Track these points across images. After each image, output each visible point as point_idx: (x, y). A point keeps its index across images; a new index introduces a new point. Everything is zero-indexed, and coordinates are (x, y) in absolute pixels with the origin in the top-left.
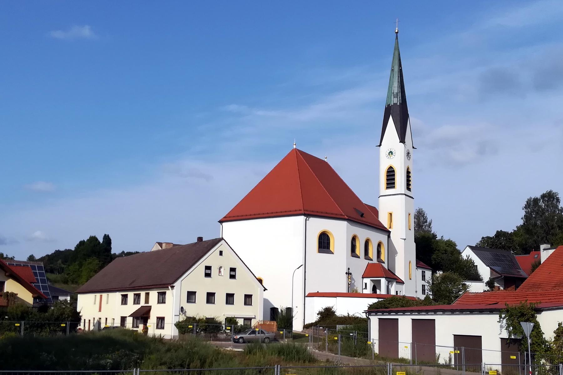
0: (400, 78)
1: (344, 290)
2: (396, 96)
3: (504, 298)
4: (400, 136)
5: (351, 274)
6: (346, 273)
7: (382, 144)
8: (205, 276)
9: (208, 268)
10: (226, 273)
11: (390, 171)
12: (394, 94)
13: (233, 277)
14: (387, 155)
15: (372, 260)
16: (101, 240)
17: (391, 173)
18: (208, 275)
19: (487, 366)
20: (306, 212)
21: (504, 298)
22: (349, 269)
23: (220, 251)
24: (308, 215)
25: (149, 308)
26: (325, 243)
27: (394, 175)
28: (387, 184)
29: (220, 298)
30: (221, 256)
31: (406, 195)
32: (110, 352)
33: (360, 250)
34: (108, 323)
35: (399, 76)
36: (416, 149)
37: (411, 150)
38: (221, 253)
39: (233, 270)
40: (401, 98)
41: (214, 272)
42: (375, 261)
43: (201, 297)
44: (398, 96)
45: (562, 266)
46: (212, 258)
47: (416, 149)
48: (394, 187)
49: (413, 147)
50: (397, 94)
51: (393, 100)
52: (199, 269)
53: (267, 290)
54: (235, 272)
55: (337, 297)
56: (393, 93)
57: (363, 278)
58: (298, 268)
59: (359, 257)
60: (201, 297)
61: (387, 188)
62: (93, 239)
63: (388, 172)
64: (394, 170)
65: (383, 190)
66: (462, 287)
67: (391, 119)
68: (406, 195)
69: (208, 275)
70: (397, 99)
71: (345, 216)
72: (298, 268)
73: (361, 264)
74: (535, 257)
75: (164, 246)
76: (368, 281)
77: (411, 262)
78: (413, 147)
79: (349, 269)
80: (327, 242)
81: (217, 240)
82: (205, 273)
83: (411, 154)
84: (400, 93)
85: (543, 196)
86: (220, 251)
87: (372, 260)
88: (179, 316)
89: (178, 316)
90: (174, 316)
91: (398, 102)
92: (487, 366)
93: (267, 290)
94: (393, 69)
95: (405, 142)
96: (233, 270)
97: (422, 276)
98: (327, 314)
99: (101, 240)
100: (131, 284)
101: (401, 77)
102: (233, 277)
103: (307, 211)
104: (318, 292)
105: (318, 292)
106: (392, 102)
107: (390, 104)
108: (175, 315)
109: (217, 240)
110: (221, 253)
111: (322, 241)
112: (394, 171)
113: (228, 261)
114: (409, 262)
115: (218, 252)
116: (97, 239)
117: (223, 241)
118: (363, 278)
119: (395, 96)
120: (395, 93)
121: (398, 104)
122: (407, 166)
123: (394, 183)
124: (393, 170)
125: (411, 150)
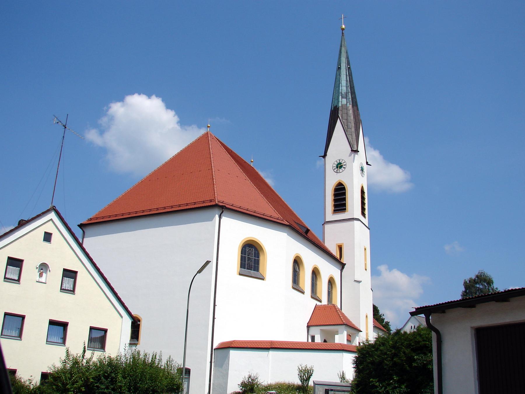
0: (349, 77)
11: (341, 209)
12: (342, 94)
14: (334, 168)
15: (320, 301)
19: (54, 341)
26: (251, 261)
28: (335, 206)
34: (16, 335)
35: (348, 74)
36: (371, 165)
37: (365, 166)
38: (48, 237)
42: (325, 302)
47: (371, 165)
49: (367, 163)
50: (347, 93)
58: (200, 271)
59: (303, 293)
61: (334, 211)
63: (336, 190)
64: (345, 187)
65: (330, 216)
66: (393, 379)
72: (200, 271)
77: (368, 316)
78: (367, 163)
83: (365, 170)
84: (350, 94)
87: (320, 301)
92: (54, 341)
94: (339, 66)
95: (359, 152)
101: (351, 83)
107: (337, 106)
110: (48, 237)
112: (344, 189)
114: (364, 249)
120: (343, 93)
125: (365, 166)
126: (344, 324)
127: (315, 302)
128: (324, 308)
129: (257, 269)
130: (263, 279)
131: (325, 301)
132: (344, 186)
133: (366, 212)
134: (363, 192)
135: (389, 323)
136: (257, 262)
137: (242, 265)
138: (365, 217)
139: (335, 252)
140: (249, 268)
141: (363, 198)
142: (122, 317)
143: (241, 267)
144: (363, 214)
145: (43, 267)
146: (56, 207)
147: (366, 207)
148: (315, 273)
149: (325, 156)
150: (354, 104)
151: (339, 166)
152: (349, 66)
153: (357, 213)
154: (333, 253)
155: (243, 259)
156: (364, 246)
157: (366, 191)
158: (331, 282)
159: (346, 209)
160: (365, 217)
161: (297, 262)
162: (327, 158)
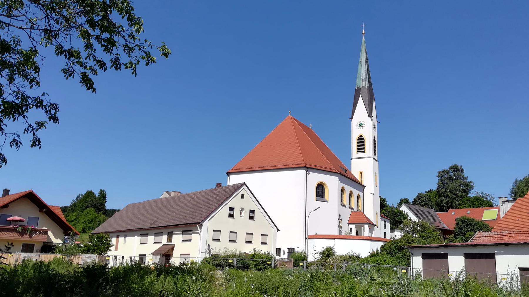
1: (336, 232)
2: (364, 81)
3: (507, 236)
4: (368, 111)
5: (341, 220)
6: (338, 219)
7: (354, 117)
8: (229, 216)
9: (231, 209)
10: (246, 214)
13: (252, 218)
14: (357, 126)
16: (97, 194)
17: (361, 141)
18: (231, 216)
20: (307, 166)
21: (507, 236)
22: (340, 216)
23: (242, 195)
24: (308, 169)
25: (173, 246)
26: (321, 193)
27: (364, 142)
29: (241, 238)
30: (242, 199)
31: (373, 158)
32: (444, 236)
33: (346, 200)
38: (243, 196)
39: (252, 211)
40: (368, 83)
41: (236, 213)
43: (225, 236)
44: (365, 81)
45: (528, 213)
46: (235, 201)
48: (364, 151)
49: (377, 121)
51: (362, 84)
52: (224, 210)
53: (279, 230)
54: (253, 214)
55: (336, 239)
56: (362, 78)
57: (348, 224)
58: (314, 211)
60: (225, 236)
61: (358, 152)
62: (90, 194)
67: (360, 99)
68: (373, 158)
69: (231, 216)
70: (365, 83)
71: (337, 171)
72: (314, 211)
73: (347, 213)
74: (468, 213)
75: (173, 194)
76: (353, 227)
77: (378, 213)
79: (340, 216)
80: (323, 192)
81: (240, 184)
82: (229, 214)
84: (368, 79)
85: (451, 168)
86: (242, 195)
88: (311, 233)
89: (205, 252)
90: (200, 252)
91: (366, 85)
93: (279, 230)
96: (252, 211)
97: (384, 225)
98: (328, 253)
99: (97, 194)
100: (152, 224)
102: (252, 218)
103: (307, 164)
104: (316, 234)
105: (316, 234)
106: (361, 85)
108: (202, 252)
109: (240, 184)
110: (243, 196)
111: (319, 191)
112: (363, 139)
113: (249, 204)
115: (240, 195)
116: (93, 194)
117: (245, 187)
118: (348, 224)
119: (364, 80)
120: (363, 79)
121: (366, 87)
122: (374, 135)
123: (364, 148)
124: (363, 138)
126: (368, 223)
127: (351, 210)
128: (140, 219)
129: (323, 196)
130: (327, 202)
131: (356, 210)
132: (363, 137)
133: (376, 152)
134: (374, 140)
135: (87, 90)
136: (324, 193)
137: (317, 196)
138: (376, 156)
139: (358, 177)
140: (320, 197)
141: (375, 144)
142: (190, 240)
143: (316, 197)
144: (375, 153)
145: (242, 210)
146: (5, 130)
147: (376, 149)
148: (351, 194)
149: (352, 119)
150: (370, 85)
151: (360, 125)
152: (367, 60)
153: (371, 154)
154: (358, 179)
155: (317, 192)
156: (376, 173)
157: (376, 139)
158: (358, 197)
159: (364, 148)
160: (376, 156)
161: (342, 191)
162: (353, 120)
